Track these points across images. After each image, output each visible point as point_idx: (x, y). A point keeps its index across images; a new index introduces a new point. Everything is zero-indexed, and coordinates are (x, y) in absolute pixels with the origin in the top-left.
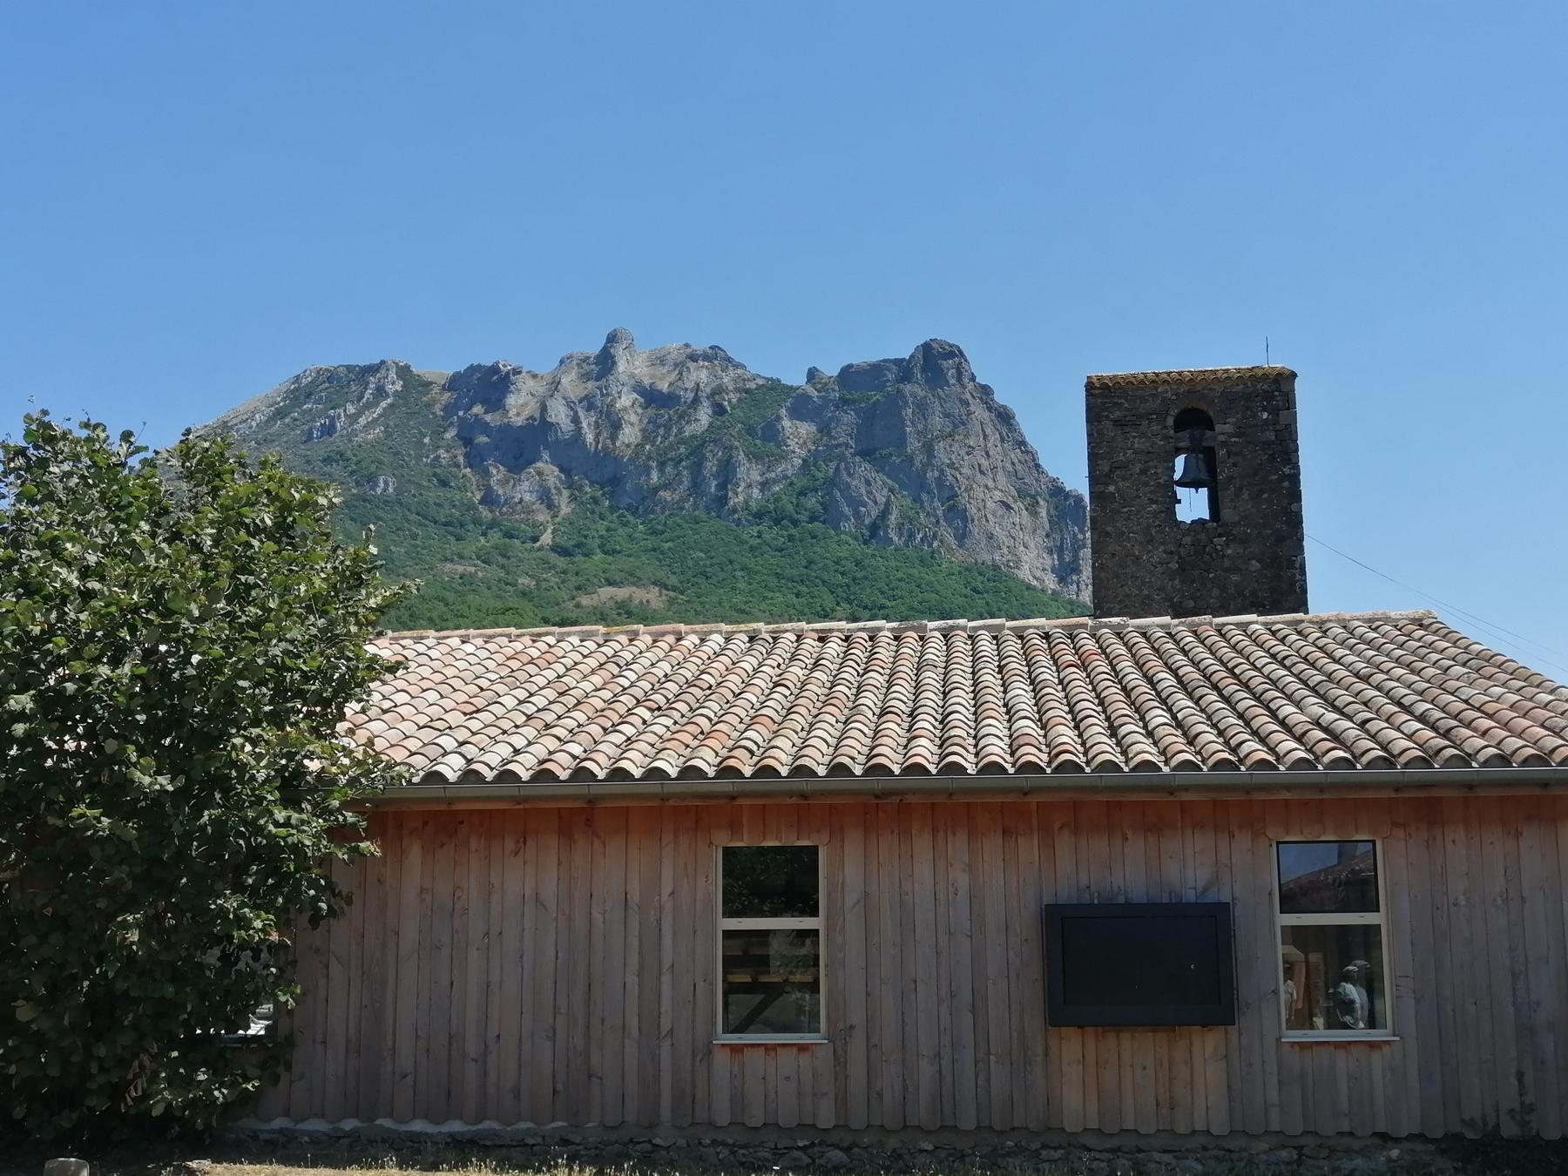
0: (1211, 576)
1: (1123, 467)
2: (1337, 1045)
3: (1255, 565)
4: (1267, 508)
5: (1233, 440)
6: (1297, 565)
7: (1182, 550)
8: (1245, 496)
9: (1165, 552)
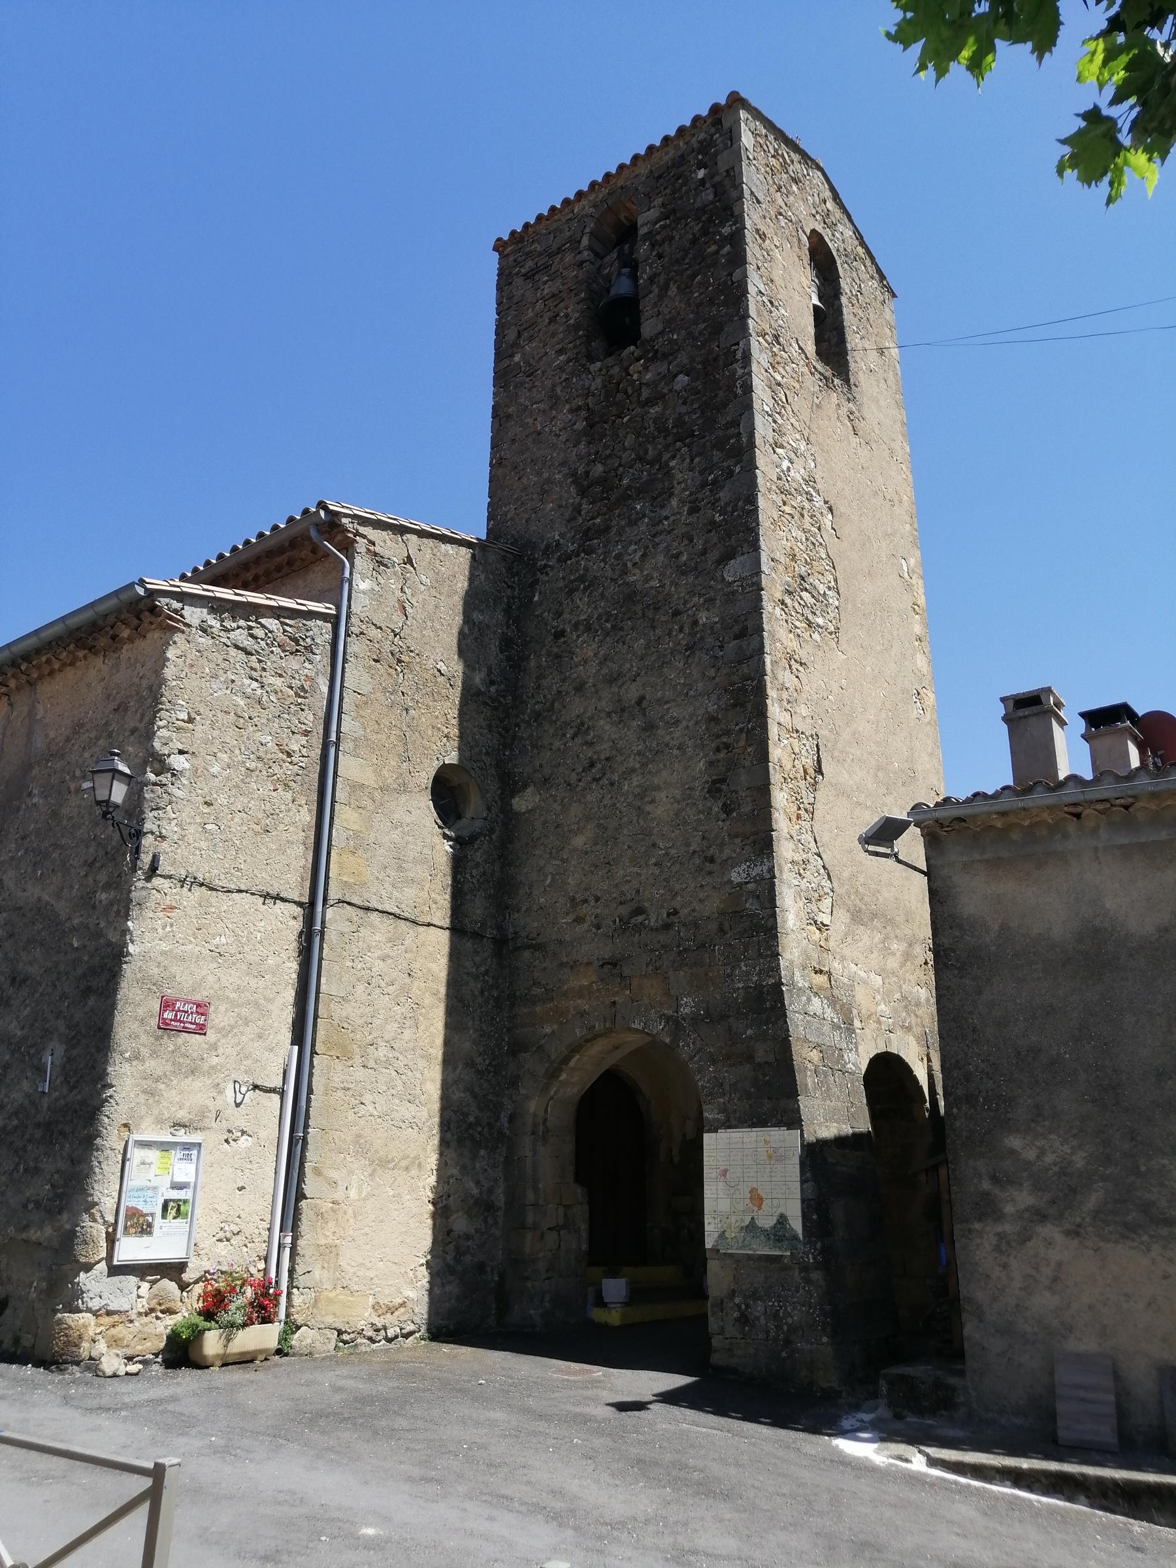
0: (626, 419)
1: (532, 325)
2: (272, 1222)
3: (682, 379)
4: (701, 294)
5: (658, 226)
6: (739, 355)
7: (590, 400)
8: (673, 290)
9: (571, 411)
